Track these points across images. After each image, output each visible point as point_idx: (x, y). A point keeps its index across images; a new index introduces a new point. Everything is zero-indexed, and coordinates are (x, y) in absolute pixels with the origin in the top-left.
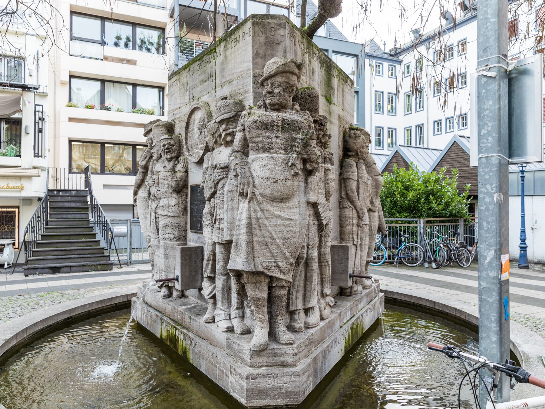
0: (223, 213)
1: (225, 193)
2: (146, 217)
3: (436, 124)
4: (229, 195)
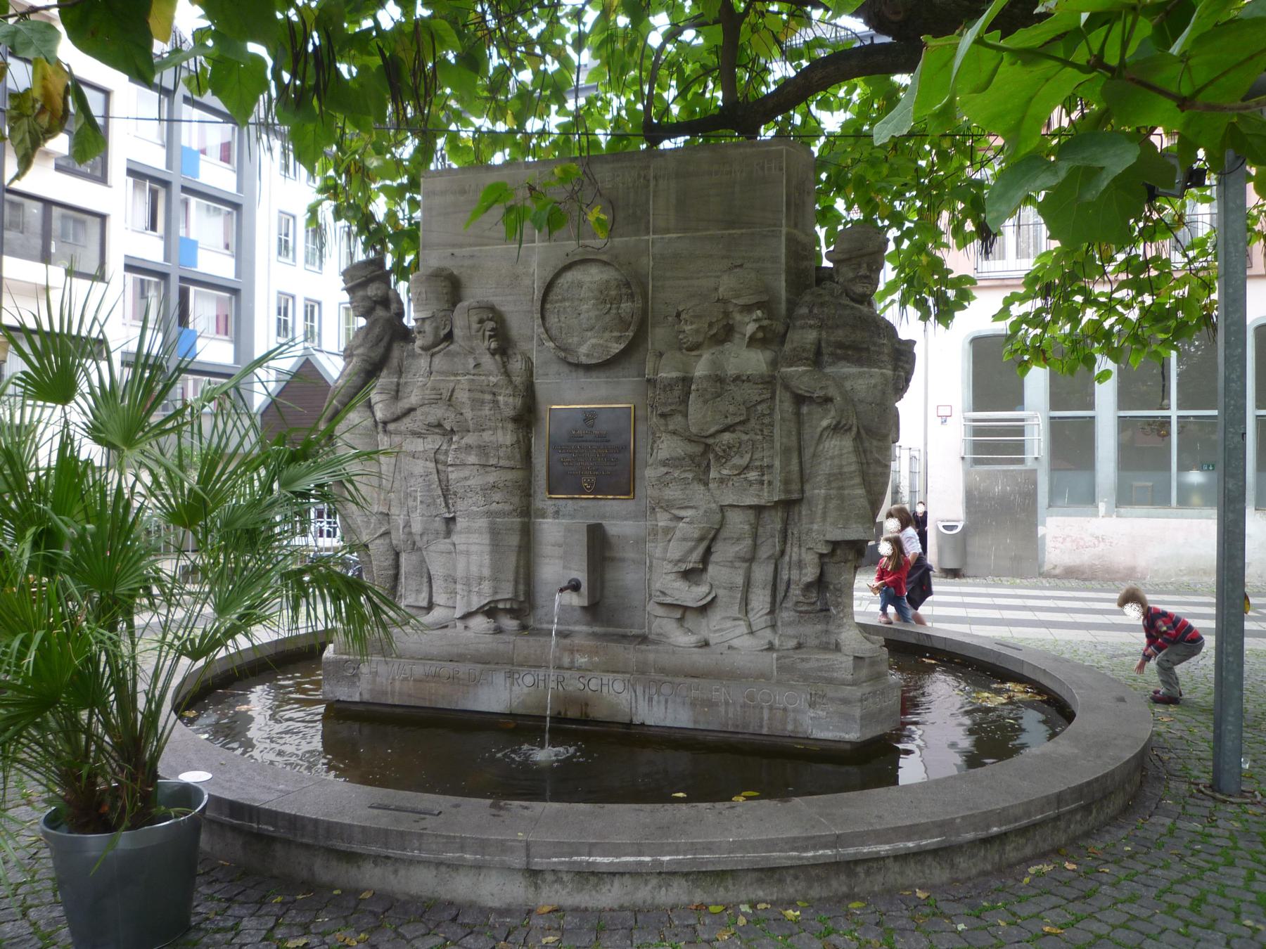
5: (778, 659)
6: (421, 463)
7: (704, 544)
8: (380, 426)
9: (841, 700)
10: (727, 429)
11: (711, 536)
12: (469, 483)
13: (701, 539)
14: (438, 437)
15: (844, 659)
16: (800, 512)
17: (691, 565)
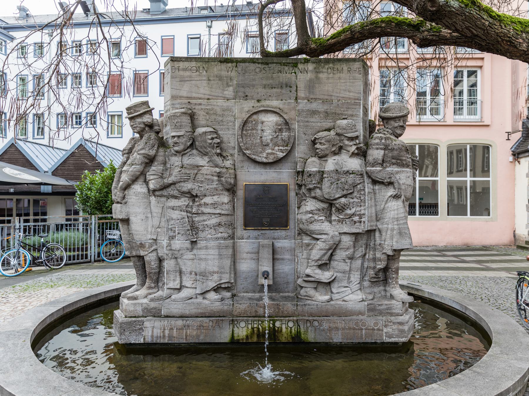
0: (365, 209)
1: (366, 194)
2: (147, 217)
3: (59, 117)
4: (369, 196)
5: (368, 305)
6: (177, 212)
7: (330, 252)
8: (151, 192)
9: (398, 323)
10: (345, 196)
11: (334, 248)
12: (206, 223)
13: (329, 249)
14: (187, 199)
15: (398, 303)
16: (374, 235)
17: (323, 262)
